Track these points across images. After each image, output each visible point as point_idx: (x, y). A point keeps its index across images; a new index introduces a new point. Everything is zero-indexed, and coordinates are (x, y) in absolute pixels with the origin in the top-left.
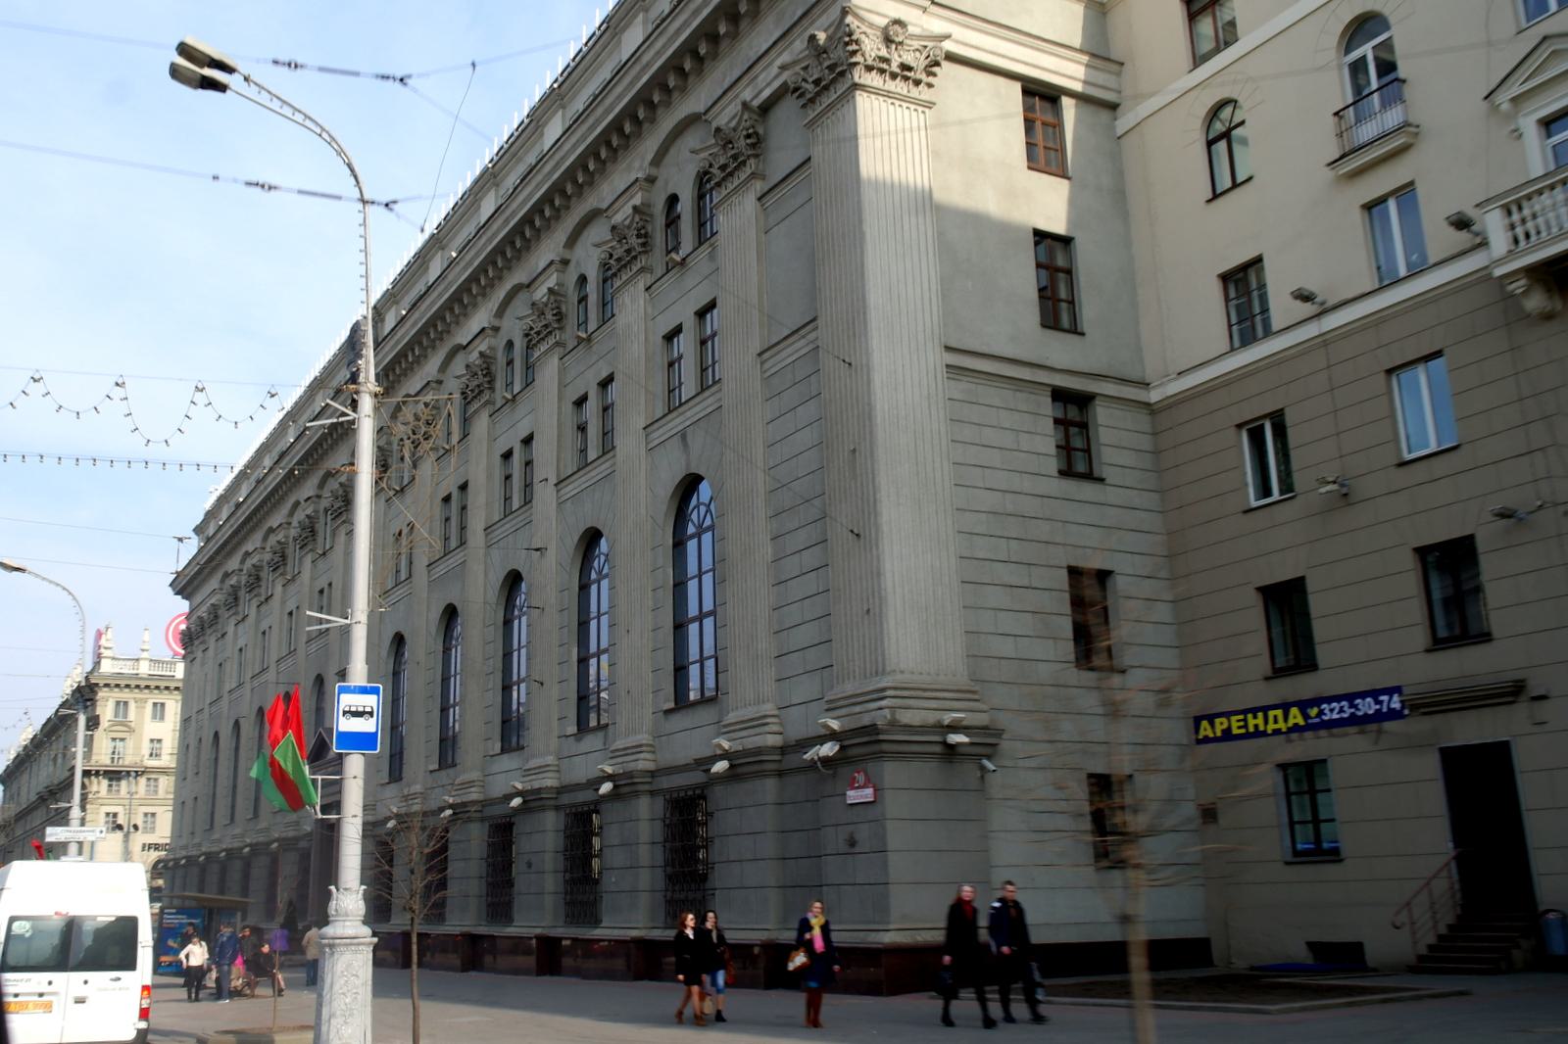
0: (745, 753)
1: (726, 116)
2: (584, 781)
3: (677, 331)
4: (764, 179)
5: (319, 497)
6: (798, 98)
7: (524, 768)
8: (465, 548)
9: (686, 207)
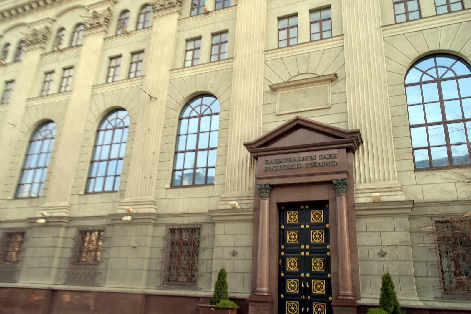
0: (138, 214)
1: (39, 27)
2: (207, 211)
3: (52, 72)
4: (180, 15)
5: (54, 21)
6: (43, 38)
7: (222, 196)
8: (143, 79)
9: (12, 49)
